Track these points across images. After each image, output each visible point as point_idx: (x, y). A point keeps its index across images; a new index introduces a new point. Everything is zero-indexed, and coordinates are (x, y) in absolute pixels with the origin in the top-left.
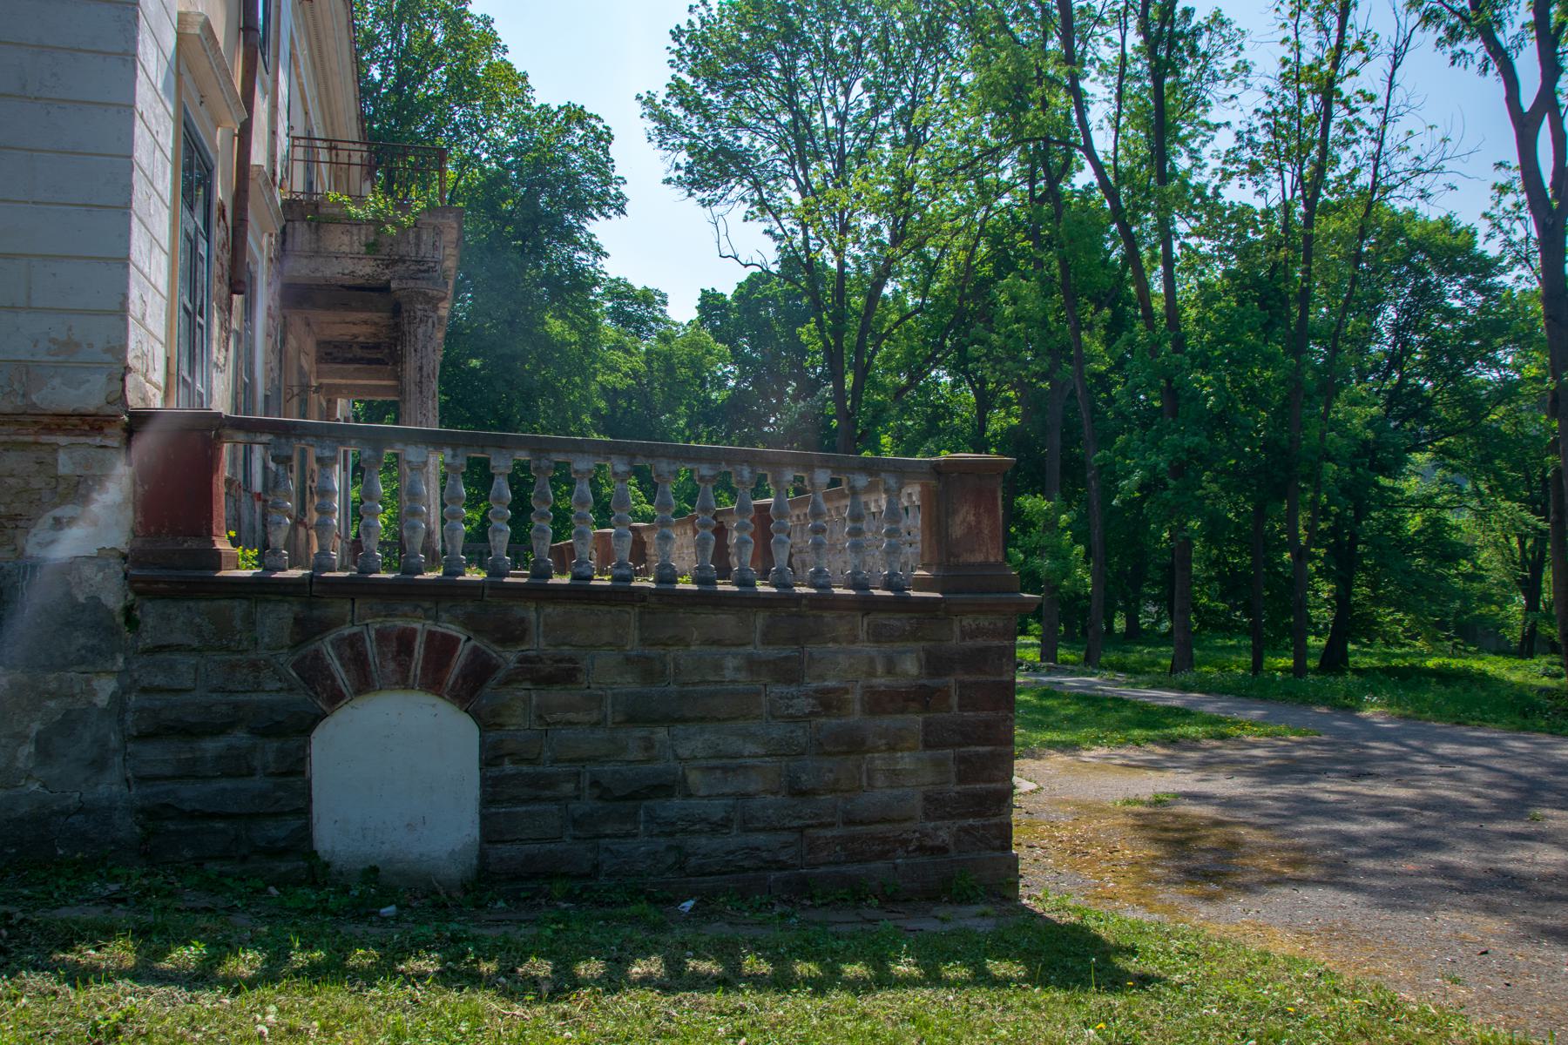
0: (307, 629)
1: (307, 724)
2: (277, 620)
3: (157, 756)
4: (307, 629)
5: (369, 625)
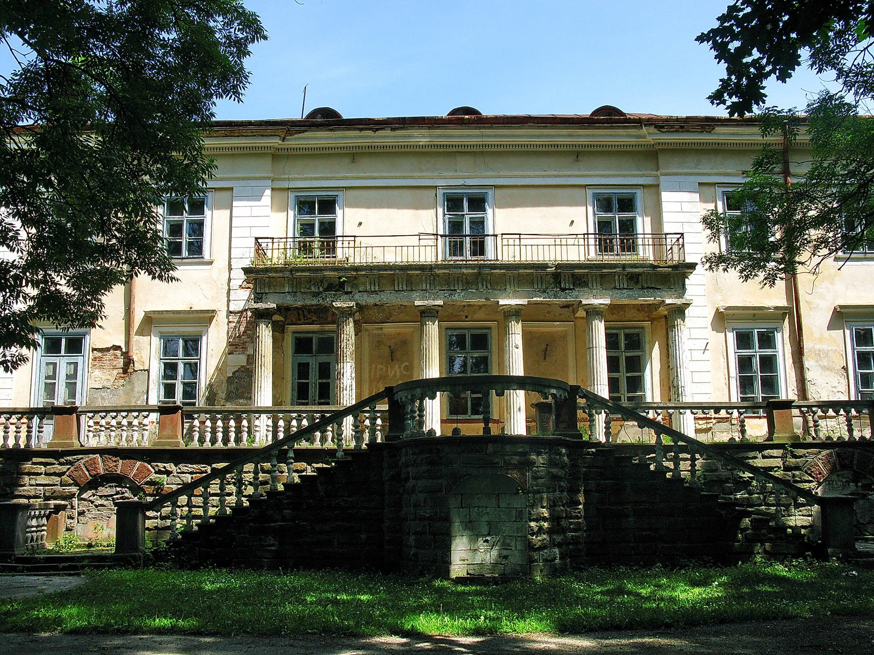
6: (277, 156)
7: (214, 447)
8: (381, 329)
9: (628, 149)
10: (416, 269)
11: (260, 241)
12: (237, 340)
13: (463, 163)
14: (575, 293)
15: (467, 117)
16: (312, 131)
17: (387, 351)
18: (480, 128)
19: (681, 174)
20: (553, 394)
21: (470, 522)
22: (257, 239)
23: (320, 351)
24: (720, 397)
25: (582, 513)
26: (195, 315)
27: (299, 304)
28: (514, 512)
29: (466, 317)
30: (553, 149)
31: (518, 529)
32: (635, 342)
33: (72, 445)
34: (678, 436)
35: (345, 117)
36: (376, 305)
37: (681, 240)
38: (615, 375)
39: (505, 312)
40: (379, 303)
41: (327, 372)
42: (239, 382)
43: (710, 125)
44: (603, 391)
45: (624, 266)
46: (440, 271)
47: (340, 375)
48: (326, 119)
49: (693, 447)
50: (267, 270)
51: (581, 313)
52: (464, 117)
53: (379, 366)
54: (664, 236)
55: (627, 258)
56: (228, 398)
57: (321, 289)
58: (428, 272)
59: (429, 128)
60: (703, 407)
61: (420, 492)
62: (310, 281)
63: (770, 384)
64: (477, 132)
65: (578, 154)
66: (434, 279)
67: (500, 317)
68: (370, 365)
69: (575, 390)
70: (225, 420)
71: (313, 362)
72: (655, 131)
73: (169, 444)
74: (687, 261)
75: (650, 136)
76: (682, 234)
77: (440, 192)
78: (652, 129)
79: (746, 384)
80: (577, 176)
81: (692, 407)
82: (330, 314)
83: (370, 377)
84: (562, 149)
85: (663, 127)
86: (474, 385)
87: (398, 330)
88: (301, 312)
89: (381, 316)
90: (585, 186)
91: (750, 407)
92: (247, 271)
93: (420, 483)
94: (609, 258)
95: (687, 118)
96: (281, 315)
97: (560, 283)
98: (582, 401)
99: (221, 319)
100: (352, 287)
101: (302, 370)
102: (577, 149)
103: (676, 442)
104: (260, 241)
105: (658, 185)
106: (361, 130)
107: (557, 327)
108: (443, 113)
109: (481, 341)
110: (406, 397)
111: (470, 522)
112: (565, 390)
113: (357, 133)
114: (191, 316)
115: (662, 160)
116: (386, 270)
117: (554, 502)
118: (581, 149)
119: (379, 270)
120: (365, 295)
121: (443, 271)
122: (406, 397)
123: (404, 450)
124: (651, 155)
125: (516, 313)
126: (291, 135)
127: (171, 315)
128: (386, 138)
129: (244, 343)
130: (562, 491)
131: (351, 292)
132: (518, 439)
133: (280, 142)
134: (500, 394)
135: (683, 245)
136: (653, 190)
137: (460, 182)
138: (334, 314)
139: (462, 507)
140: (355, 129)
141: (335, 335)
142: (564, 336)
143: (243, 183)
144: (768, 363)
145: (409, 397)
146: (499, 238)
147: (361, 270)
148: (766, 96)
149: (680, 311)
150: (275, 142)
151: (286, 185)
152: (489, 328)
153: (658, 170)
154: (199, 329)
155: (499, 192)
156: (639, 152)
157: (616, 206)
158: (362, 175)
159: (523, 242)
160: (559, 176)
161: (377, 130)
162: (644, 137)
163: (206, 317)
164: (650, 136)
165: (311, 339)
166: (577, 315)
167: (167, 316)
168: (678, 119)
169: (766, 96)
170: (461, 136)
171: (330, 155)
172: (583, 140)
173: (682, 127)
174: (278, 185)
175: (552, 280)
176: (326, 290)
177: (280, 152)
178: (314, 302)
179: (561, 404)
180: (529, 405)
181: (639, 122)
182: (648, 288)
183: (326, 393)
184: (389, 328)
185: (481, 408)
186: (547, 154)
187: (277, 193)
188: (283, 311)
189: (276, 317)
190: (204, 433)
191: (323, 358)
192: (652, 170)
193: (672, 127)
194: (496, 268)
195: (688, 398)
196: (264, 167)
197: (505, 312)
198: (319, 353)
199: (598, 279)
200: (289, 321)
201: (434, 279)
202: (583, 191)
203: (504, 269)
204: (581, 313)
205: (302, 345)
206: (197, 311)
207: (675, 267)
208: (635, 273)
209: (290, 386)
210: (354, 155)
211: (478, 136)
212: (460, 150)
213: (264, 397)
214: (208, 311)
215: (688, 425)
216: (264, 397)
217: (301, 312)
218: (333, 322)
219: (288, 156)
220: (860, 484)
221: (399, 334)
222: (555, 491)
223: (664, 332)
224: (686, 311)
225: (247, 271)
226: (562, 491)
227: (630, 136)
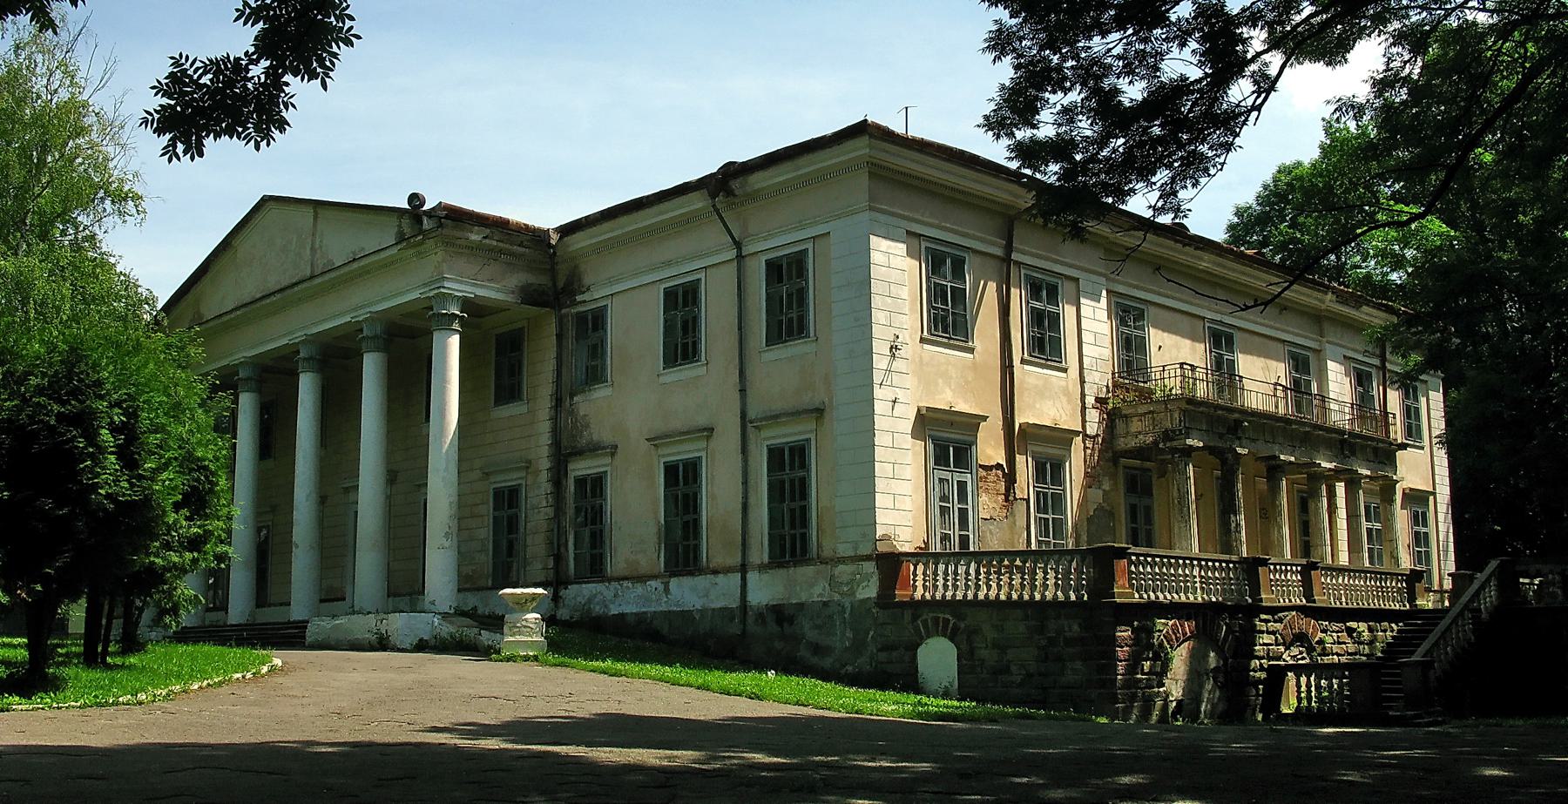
0: (915, 618)
1: (919, 645)
2: (908, 615)
3: (883, 656)
4: (915, 618)
5: (928, 616)
115: (1326, 326)
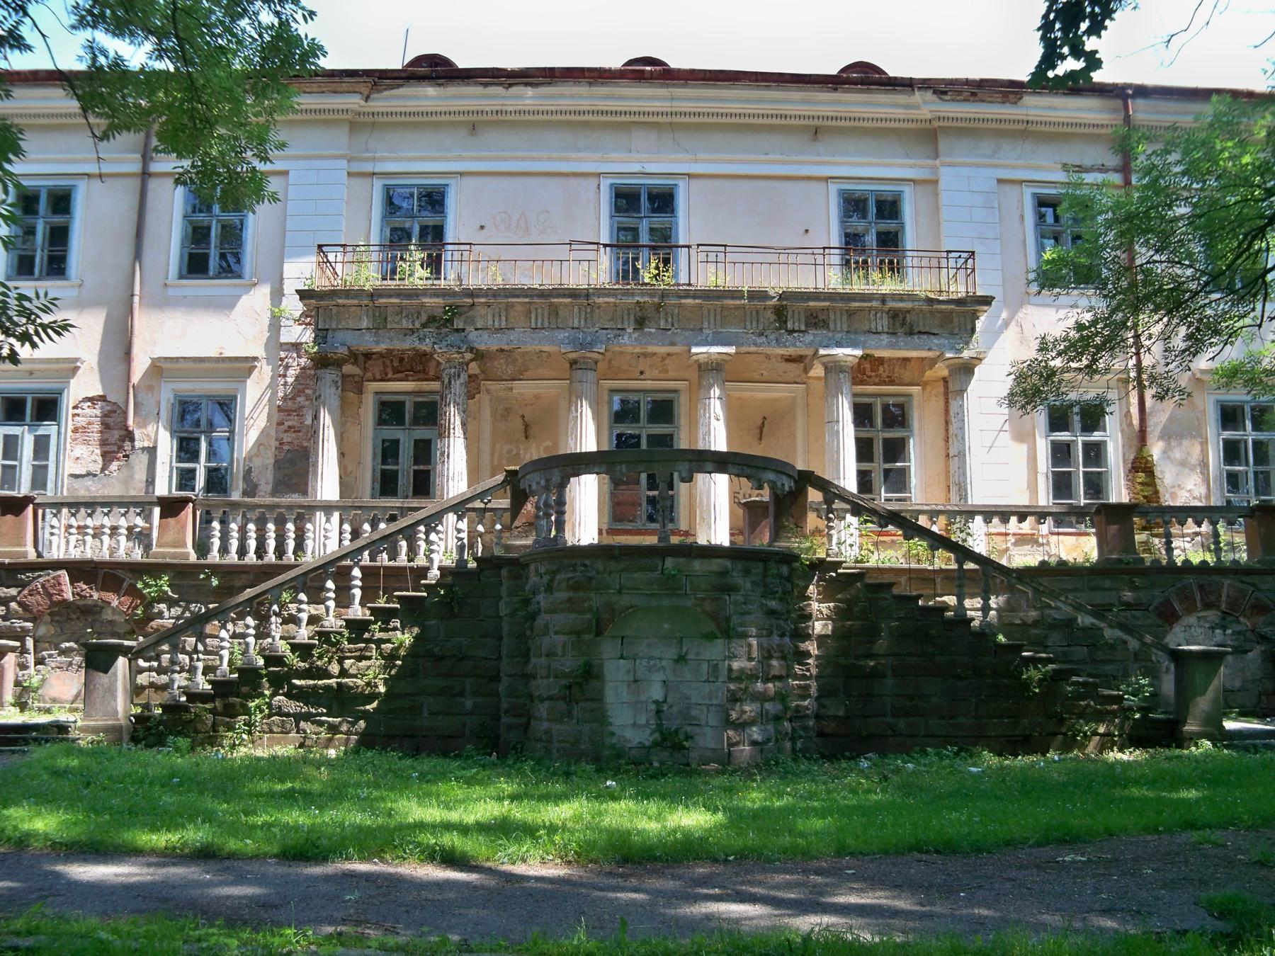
6: (357, 124)
7: (241, 562)
8: (511, 389)
9: (892, 125)
10: (564, 296)
11: (325, 249)
12: (290, 403)
13: (640, 139)
14: (809, 338)
15: (649, 68)
16: (410, 86)
17: (517, 424)
18: (667, 86)
19: (970, 165)
20: (769, 482)
21: (635, 681)
22: (320, 247)
23: (417, 421)
24: (1021, 499)
25: (814, 671)
26: (227, 365)
27: (382, 347)
28: (705, 667)
29: (642, 373)
30: (778, 121)
31: (710, 692)
32: (898, 417)
33: (25, 554)
34: (963, 553)
35: (461, 64)
36: (502, 351)
37: (970, 261)
38: (866, 466)
39: (700, 366)
40: (506, 347)
41: (425, 452)
42: (294, 466)
43: (1016, 93)
44: (850, 483)
45: (884, 298)
46: (601, 300)
47: (445, 455)
48: (433, 69)
49: (989, 574)
50: (333, 294)
51: (818, 371)
52: (646, 71)
53: (507, 447)
54: (945, 255)
55: (888, 286)
56: (274, 493)
57: (417, 325)
58: (583, 301)
59: (590, 84)
60: (1004, 514)
61: (556, 633)
62: (400, 310)
63: (1096, 485)
64: (663, 92)
65: (816, 132)
66: (592, 311)
67: (693, 374)
68: (493, 446)
69: (807, 479)
70: (280, 523)
71: (406, 437)
72: (934, 98)
73: (174, 556)
74: (978, 294)
75: (926, 107)
76: (973, 253)
77: (605, 183)
78: (929, 95)
79: (1062, 485)
80: (816, 163)
81: (989, 514)
82: (432, 365)
83: (492, 461)
84: (792, 122)
85: (945, 93)
86: (647, 457)
87: (535, 391)
88: (388, 362)
89: (510, 370)
90: (827, 179)
91: (1066, 518)
92: (303, 295)
93: (555, 617)
94: (858, 286)
95: (982, 81)
96: (356, 363)
97: (786, 322)
98: (814, 495)
99: (264, 372)
100: (465, 322)
101: (389, 451)
102: (816, 122)
103: (960, 562)
104: (325, 249)
105: (935, 182)
106: (486, 85)
107: (780, 392)
108: (616, 63)
109: (663, 410)
110: (538, 483)
111: (635, 681)
112: (790, 476)
113: (479, 90)
114: (220, 365)
115: (943, 144)
116: (518, 296)
117: (769, 651)
118: (820, 123)
119: (507, 297)
120: (485, 335)
121: (607, 299)
122: (538, 483)
123: (532, 567)
124: (928, 137)
125: (713, 369)
126: (379, 91)
127: (191, 365)
128: (527, 97)
129: (301, 408)
130: (782, 635)
131: (464, 330)
132: (712, 552)
133: (362, 103)
134: (689, 479)
135: (973, 270)
136: (929, 188)
137: (636, 168)
138: (439, 363)
139: (622, 657)
140: (477, 84)
141: (438, 397)
142: (791, 407)
143: (302, 164)
144: (1095, 453)
145: (543, 482)
146: (693, 252)
147: (478, 297)
148: (1096, 52)
149: (966, 370)
150: (353, 102)
151: (369, 168)
152: (676, 391)
153: (936, 156)
154: (233, 385)
155: (695, 183)
156: (909, 131)
157: (872, 210)
158: (486, 154)
159: (730, 257)
160: (790, 163)
161: (510, 85)
162: (917, 107)
163: (245, 366)
164: (926, 107)
165: (403, 403)
166: (812, 373)
167: (183, 365)
168: (967, 82)
169: (1096, 52)
170: (637, 98)
171: (438, 126)
172: (824, 110)
173: (973, 94)
174: (357, 167)
175: (773, 317)
176: (424, 326)
177: (362, 119)
178: (406, 346)
179: (784, 493)
180: (734, 495)
181: (907, 85)
182: (920, 332)
183: (423, 485)
184: (524, 389)
185: (662, 509)
186: (771, 129)
187: (357, 182)
188: (361, 358)
189: (348, 369)
190: (233, 545)
191: (422, 433)
192: (928, 157)
193: (959, 93)
194: (686, 297)
195: (979, 496)
196: (339, 139)
197: (700, 366)
198: (415, 424)
199: (845, 317)
200: (369, 375)
201: (592, 311)
202: (822, 185)
203: (699, 298)
204: (818, 371)
205: (390, 412)
206: (230, 359)
207: (959, 302)
208: (900, 310)
209: (369, 475)
210: (475, 125)
211: (665, 99)
212: (637, 118)
213: (327, 486)
214: (246, 359)
215: (979, 538)
216: (327, 486)
217: (388, 362)
218: (437, 378)
219: (373, 126)
220: (1229, 631)
221: (537, 397)
222: (770, 634)
223: (942, 403)
224: (976, 370)
225: (303, 295)
226: (782, 635)
227: (896, 105)
